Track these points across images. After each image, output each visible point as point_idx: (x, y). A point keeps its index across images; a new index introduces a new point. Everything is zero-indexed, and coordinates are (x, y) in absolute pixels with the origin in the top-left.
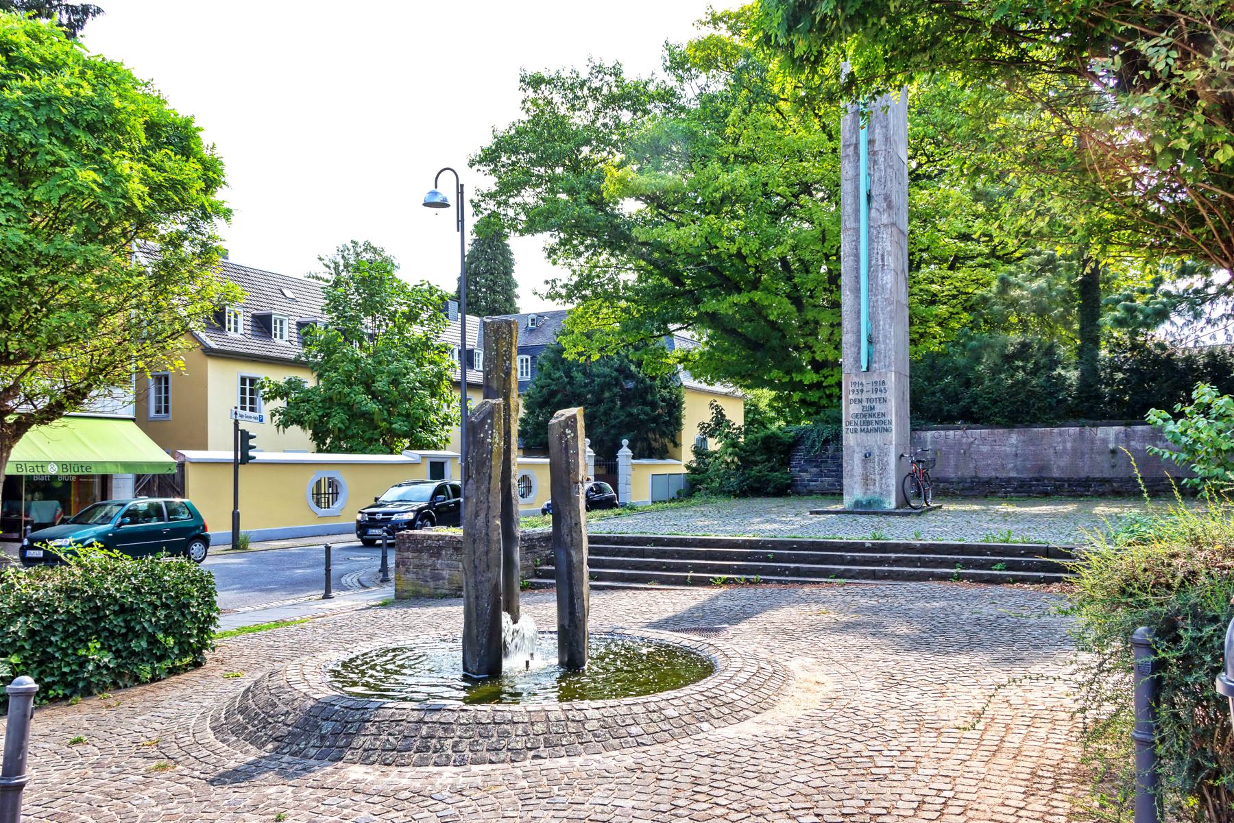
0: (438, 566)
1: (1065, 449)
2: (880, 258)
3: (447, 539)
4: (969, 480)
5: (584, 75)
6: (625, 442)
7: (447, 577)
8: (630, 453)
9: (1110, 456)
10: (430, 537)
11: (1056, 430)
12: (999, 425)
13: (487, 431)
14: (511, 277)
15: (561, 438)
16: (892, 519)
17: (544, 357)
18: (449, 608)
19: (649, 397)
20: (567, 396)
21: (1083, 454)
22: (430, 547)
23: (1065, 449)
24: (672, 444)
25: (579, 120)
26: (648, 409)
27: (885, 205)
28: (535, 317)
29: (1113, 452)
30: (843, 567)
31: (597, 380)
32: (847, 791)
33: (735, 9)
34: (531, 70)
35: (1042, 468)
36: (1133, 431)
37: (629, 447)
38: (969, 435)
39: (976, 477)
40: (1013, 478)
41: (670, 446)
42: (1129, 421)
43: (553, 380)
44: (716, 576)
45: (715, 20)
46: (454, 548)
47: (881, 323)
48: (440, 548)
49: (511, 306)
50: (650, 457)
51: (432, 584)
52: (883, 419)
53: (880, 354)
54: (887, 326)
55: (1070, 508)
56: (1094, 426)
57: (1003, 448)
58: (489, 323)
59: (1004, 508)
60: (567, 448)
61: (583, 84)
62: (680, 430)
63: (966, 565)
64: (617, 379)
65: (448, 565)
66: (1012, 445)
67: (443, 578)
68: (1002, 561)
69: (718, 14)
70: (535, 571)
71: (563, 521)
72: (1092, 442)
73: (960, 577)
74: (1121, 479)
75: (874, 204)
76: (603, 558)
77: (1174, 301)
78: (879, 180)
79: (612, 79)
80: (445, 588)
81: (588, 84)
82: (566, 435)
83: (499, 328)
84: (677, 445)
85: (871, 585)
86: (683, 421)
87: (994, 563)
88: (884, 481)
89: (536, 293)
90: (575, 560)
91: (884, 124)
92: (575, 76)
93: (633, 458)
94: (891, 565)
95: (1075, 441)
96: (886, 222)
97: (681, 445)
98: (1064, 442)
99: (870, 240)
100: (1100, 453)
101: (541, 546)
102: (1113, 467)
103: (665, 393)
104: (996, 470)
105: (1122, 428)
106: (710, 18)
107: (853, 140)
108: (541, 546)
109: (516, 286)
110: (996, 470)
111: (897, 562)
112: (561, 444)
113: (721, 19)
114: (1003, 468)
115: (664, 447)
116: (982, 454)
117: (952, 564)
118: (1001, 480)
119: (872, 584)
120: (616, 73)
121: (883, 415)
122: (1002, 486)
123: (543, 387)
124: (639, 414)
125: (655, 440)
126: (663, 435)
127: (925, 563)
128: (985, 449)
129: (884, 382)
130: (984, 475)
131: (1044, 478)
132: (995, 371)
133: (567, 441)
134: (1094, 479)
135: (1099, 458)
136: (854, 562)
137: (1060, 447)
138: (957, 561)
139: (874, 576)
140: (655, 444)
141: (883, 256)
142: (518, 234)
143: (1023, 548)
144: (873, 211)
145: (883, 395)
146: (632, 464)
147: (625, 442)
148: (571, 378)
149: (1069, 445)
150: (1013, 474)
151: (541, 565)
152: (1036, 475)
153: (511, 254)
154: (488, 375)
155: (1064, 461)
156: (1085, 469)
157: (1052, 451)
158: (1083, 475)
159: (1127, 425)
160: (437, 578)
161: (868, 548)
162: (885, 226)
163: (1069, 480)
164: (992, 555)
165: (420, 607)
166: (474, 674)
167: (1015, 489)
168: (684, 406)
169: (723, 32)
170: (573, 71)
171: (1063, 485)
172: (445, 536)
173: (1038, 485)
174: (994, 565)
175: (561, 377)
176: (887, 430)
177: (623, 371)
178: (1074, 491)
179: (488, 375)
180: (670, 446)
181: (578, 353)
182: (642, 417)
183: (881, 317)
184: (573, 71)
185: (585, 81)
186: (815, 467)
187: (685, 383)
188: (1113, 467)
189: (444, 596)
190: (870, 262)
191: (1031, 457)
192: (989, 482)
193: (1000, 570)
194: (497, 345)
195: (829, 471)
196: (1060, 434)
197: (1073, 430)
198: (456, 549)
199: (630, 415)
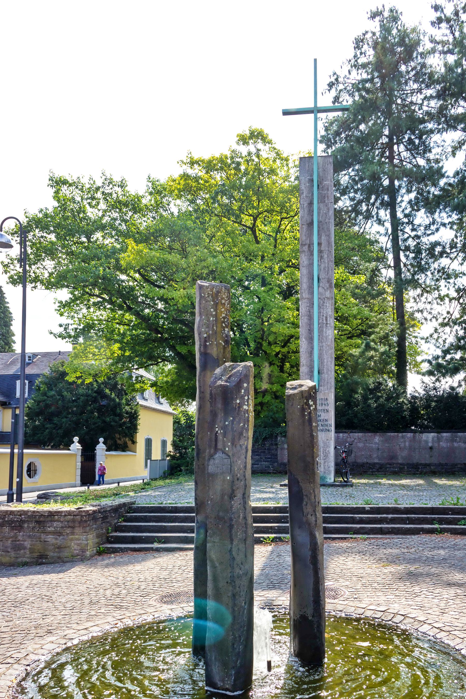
0: (20, 538)
2: (324, 319)
3: (30, 514)
4: (351, 464)
5: (99, 183)
6: (101, 440)
7: (29, 546)
8: (104, 447)
9: (430, 450)
10: (12, 512)
11: (400, 435)
12: (369, 431)
13: (242, 397)
14: (10, 329)
15: (303, 410)
16: (331, 489)
17: (41, 382)
19: (118, 411)
20: (58, 408)
22: (13, 522)
23: (405, 445)
24: (130, 442)
25: (92, 213)
26: (117, 418)
27: (328, 285)
28: (31, 355)
29: (431, 448)
31: (82, 398)
32: (117, 626)
33: (207, 157)
34: (60, 173)
37: (104, 443)
38: (352, 437)
39: (355, 462)
40: (377, 463)
41: (129, 443)
42: (439, 430)
43: (48, 397)
44: (265, 536)
45: (192, 163)
46: (37, 522)
47: (325, 361)
48: (22, 521)
49: (9, 348)
50: (116, 450)
51: (13, 554)
52: (326, 423)
53: (325, 381)
54: (329, 363)
57: (371, 445)
58: (207, 287)
60: (310, 421)
61: (98, 189)
62: (136, 433)
63: (441, 521)
64: (95, 398)
65: (30, 537)
66: (376, 443)
67: (25, 548)
69: (196, 158)
70: (108, 538)
71: (306, 499)
72: (420, 442)
73: (442, 531)
75: (321, 285)
76: (177, 524)
78: (324, 269)
79: (119, 190)
80: (26, 556)
81: (101, 190)
82: (309, 406)
83: (218, 292)
84: (134, 442)
85: (397, 539)
86: (139, 427)
87: (459, 520)
88: (326, 464)
89: (51, 333)
90: (319, 542)
91: (327, 233)
92: (92, 183)
93: (107, 451)
94: (388, 523)
95: (410, 441)
96: (328, 296)
97: (136, 442)
98: (405, 442)
99: (319, 307)
101: (112, 517)
102: (431, 457)
103: (127, 408)
104: (366, 458)
105: (436, 434)
106: (189, 161)
107: (308, 242)
108: (112, 517)
109: (13, 335)
110: (366, 458)
111: (393, 521)
112: (304, 415)
113: (197, 162)
114: (371, 457)
115: (125, 443)
116: (359, 448)
117: (431, 522)
118: (370, 464)
119: (386, 538)
120: (122, 185)
121: (326, 420)
122: (370, 468)
123: (40, 402)
124: (111, 422)
125: (120, 439)
126: (126, 436)
127: (412, 521)
128: (361, 445)
129: (327, 399)
130: (359, 461)
131: (394, 463)
132: (365, 398)
133: (310, 413)
134: (421, 464)
136: (361, 521)
137: (402, 445)
138: (434, 519)
139: (381, 531)
140: (119, 442)
141: (326, 317)
142: (43, 287)
144: (320, 288)
145: (326, 408)
146: (106, 455)
147: (101, 440)
148: (62, 396)
149: (407, 444)
150: (376, 461)
151: (111, 533)
152: (389, 461)
153: (11, 313)
154: (206, 341)
156: (417, 458)
157: (398, 447)
158: (415, 461)
159: (438, 432)
160: (17, 547)
161: (368, 511)
162: (328, 298)
163: (408, 464)
164: (452, 514)
165: (8, 576)
166: (227, 690)
167: (378, 470)
168: (139, 417)
169: (197, 171)
170: (91, 179)
171: (404, 468)
172: (28, 511)
175: (54, 395)
176: (328, 431)
177: (100, 393)
178: (410, 471)
179: (206, 341)
180: (129, 443)
181: (76, 377)
182: (112, 423)
183: (325, 357)
184: (91, 179)
185: (99, 187)
186: (257, 455)
187: (140, 403)
188: (431, 457)
189: (25, 564)
190: (319, 320)
191: (386, 451)
192: (363, 465)
194: (216, 310)
195: (266, 458)
196: (403, 437)
198: (38, 522)
199: (104, 422)
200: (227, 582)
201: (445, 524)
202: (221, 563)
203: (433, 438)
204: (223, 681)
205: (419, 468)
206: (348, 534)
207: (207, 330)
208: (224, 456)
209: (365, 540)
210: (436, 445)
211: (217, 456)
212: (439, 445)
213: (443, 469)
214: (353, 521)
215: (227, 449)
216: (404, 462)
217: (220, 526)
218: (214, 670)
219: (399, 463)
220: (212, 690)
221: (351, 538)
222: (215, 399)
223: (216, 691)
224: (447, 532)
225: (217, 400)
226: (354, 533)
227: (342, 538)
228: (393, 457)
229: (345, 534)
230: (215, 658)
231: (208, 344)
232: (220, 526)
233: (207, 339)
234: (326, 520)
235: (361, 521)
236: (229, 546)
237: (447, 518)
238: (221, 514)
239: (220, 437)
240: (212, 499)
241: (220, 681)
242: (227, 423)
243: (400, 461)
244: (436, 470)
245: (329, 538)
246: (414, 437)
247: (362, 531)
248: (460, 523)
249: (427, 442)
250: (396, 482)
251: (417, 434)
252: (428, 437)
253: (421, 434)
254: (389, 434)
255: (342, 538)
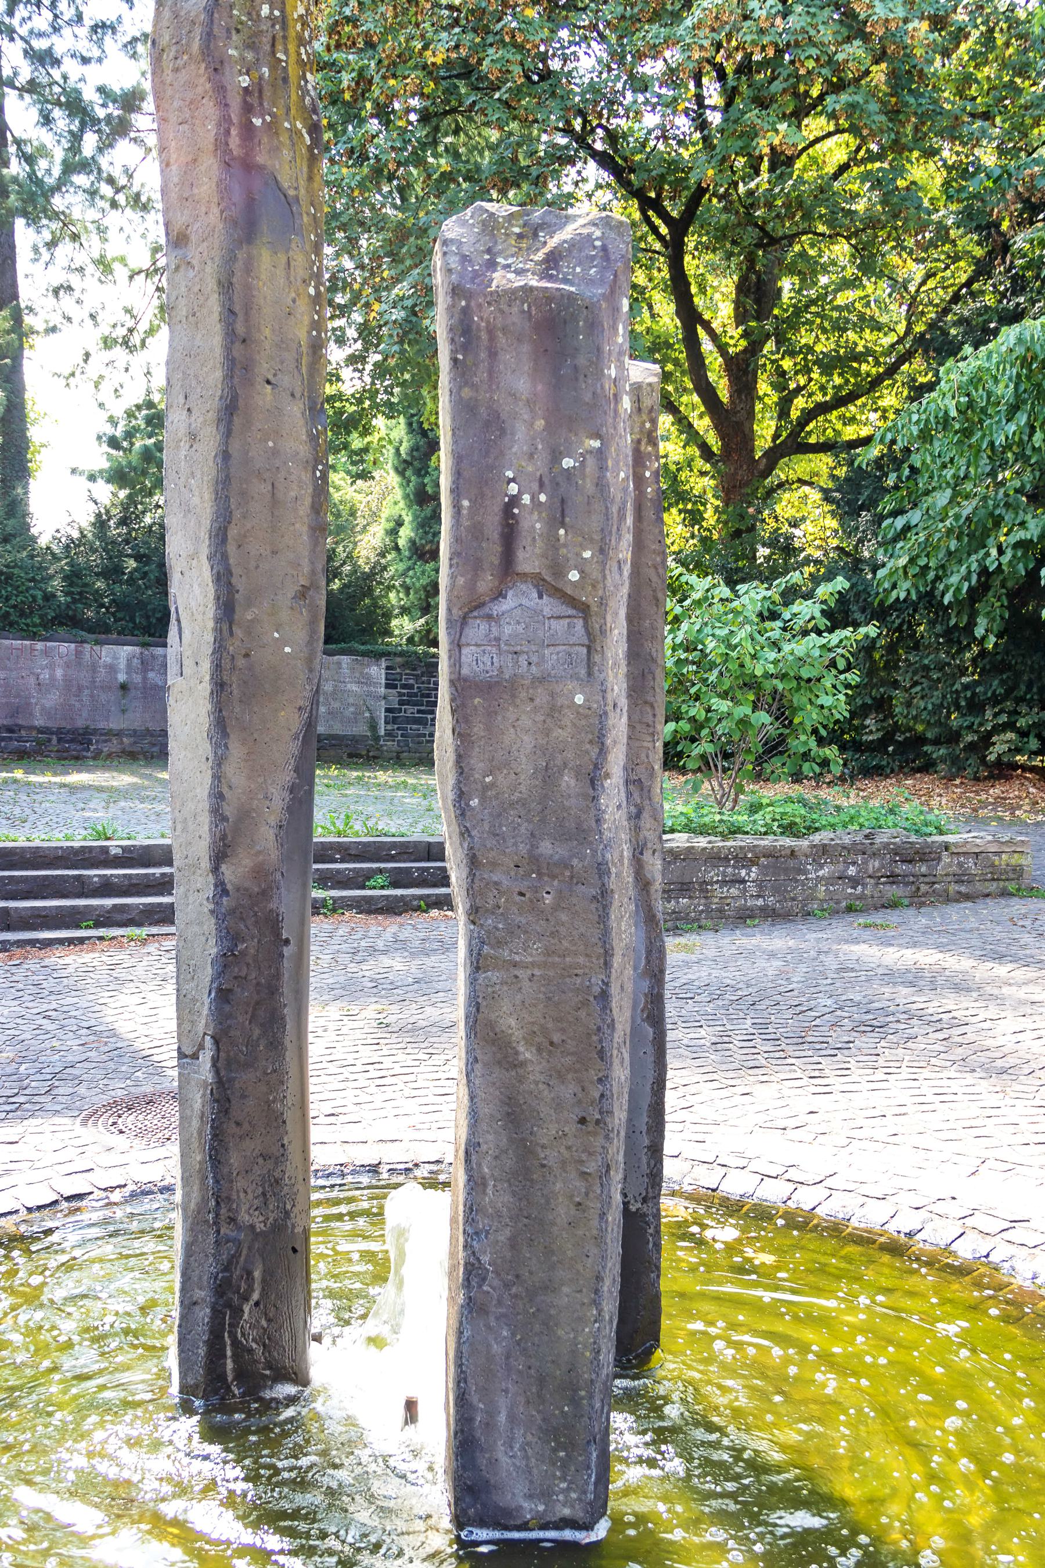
1: (52, 678)
9: (120, 693)
11: (40, 645)
18: (205, 1011)
21: (80, 689)
23: (52, 678)
29: (124, 687)
30: (109, 902)
35: (16, 712)
36: (153, 656)
42: (147, 639)
55: (124, 779)
56: (97, 642)
59: (382, 776)
68: (381, 871)
72: (94, 668)
74: (135, 731)
77: (934, 582)
87: (369, 875)
95: (68, 665)
98: (52, 667)
100: (106, 688)
105: (137, 649)
131: (21, 727)
135: (103, 697)
136: (106, 888)
137: (45, 675)
143: (394, 845)
149: (59, 673)
155: (52, 699)
157: (32, 680)
158: (80, 723)
159: (144, 645)
161: (116, 857)
163: (59, 731)
171: (49, 740)
173: (10, 738)
174: (369, 879)
178: (67, 750)
193: (382, 888)
196: (46, 653)
197: (66, 648)
200: (583, 1121)
201: (332, 888)
202: (549, 1047)
203: (129, 661)
204: (546, 1495)
205: (90, 742)
206: (78, 927)
207: (249, 56)
208: (548, 605)
209: (144, 942)
210: (137, 679)
211: (508, 603)
212: (145, 679)
213: (154, 745)
214: (83, 888)
215: (574, 576)
216: (50, 724)
217: (548, 899)
218: (504, 1460)
219: (34, 728)
220: (497, 1535)
221: (101, 938)
222: (493, 354)
223: (516, 1535)
224: (350, 907)
225: (507, 357)
226: (98, 925)
227: (71, 941)
228: (21, 708)
229: (68, 927)
230: (512, 1418)
231: (257, 122)
232: (548, 899)
233: (253, 100)
234: (165, 885)
235: (106, 888)
236: (597, 980)
237: (338, 871)
238: (546, 847)
239: (533, 524)
240: (486, 787)
241: (530, 1497)
242: (567, 463)
243: (39, 722)
244: (137, 748)
245: (32, 943)
246: (78, 654)
247: (118, 917)
248: (372, 883)
249: (112, 669)
250: (57, 779)
251: (87, 646)
252: (115, 658)
253: (97, 648)
254: (7, 642)
255: (71, 941)
